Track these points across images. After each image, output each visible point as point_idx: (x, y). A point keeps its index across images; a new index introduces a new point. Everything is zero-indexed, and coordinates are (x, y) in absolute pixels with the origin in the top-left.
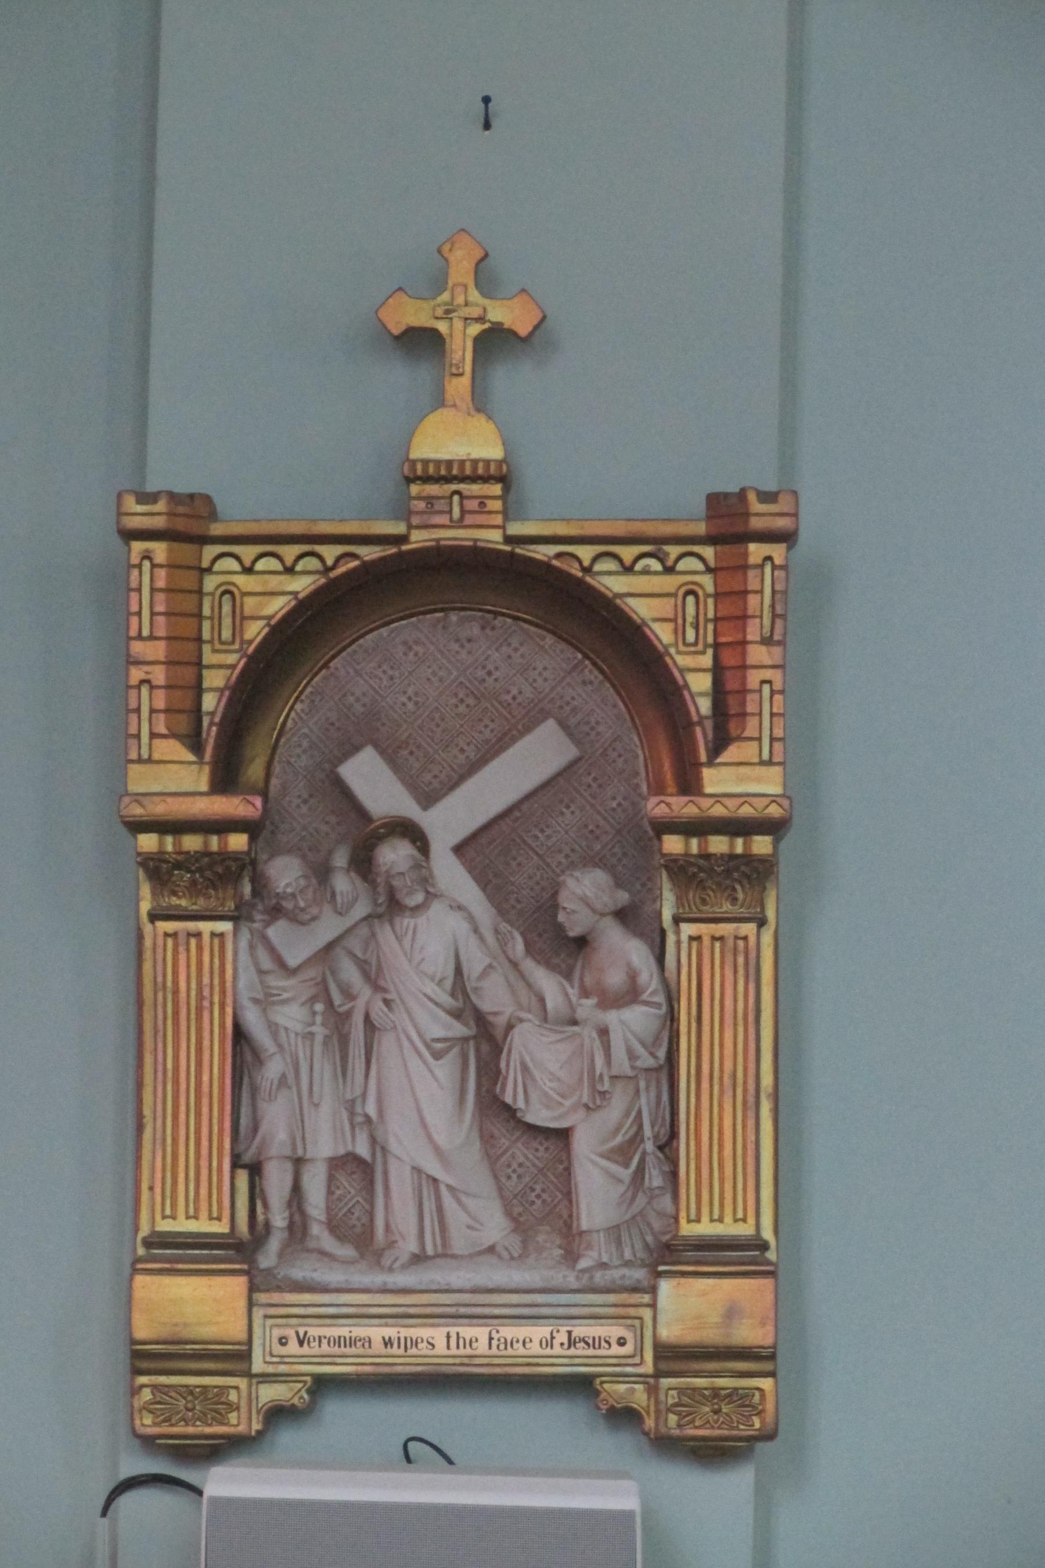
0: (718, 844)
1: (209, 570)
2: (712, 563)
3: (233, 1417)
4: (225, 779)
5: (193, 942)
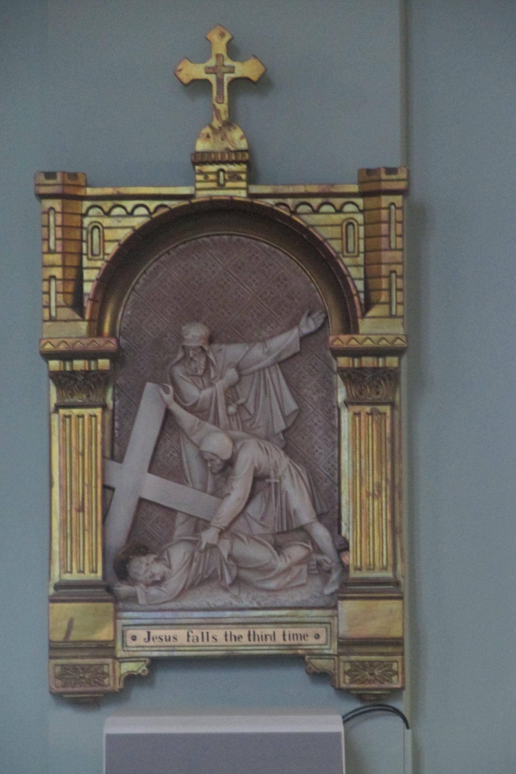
0: (368, 362)
1: (85, 215)
2: (361, 208)
3: (394, 678)
4: (96, 330)
5: (68, 420)
